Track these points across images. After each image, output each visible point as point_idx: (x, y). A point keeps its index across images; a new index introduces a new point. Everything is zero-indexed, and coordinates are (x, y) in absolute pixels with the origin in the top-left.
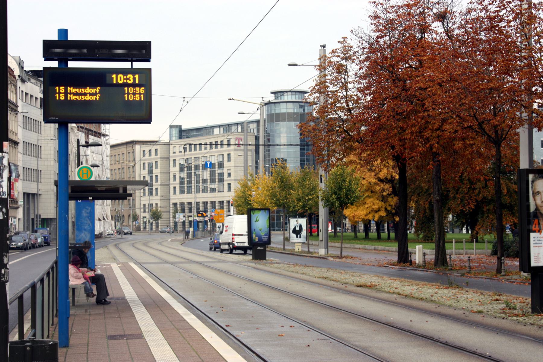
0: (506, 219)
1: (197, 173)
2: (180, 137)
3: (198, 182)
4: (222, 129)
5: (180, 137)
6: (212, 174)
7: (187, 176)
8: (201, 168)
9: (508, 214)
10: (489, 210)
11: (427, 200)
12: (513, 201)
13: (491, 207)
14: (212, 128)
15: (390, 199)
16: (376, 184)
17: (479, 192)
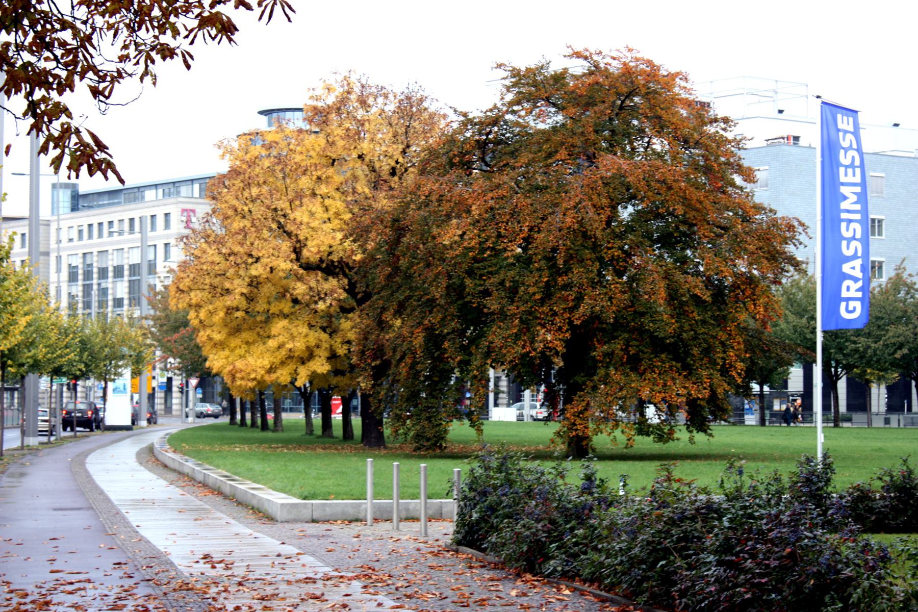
0: (665, 385)
1: (103, 285)
2: (74, 208)
3: (102, 304)
4: (160, 191)
5: (74, 208)
6: (134, 287)
7: (84, 291)
8: (111, 274)
9: (671, 367)
10: (610, 355)
11: (420, 324)
12: (687, 327)
13: (617, 346)
14: (141, 189)
15: (345, 324)
16: (290, 274)
17: (579, 299)
